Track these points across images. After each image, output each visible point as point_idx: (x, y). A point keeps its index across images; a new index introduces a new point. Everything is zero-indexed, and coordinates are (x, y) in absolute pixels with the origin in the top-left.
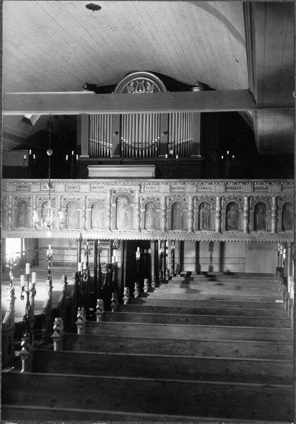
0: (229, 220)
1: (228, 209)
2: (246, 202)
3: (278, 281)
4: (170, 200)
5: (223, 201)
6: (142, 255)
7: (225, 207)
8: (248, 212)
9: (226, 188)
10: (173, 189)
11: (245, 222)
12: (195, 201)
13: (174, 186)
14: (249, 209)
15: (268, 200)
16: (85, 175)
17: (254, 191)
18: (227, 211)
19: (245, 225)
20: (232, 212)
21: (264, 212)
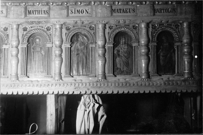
0: (118, 60)
1: (116, 43)
2: (144, 31)
3: (99, 29)
4: (25, 29)
5: (107, 30)
6: (186, 44)
7: (112, 40)
8: (147, 46)
9: (112, 11)
10: (30, 13)
11: (100, 63)
12: (64, 31)
13: (30, 9)
14: (149, 41)
15: (177, 26)
16: (161, 76)
17: (154, 15)
18: (115, 46)
19: (144, 65)
20: (122, 48)
21: (171, 46)
